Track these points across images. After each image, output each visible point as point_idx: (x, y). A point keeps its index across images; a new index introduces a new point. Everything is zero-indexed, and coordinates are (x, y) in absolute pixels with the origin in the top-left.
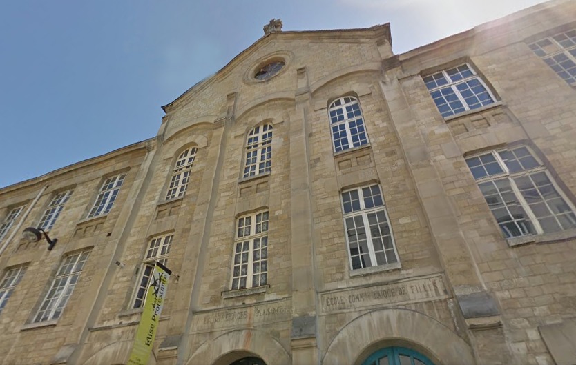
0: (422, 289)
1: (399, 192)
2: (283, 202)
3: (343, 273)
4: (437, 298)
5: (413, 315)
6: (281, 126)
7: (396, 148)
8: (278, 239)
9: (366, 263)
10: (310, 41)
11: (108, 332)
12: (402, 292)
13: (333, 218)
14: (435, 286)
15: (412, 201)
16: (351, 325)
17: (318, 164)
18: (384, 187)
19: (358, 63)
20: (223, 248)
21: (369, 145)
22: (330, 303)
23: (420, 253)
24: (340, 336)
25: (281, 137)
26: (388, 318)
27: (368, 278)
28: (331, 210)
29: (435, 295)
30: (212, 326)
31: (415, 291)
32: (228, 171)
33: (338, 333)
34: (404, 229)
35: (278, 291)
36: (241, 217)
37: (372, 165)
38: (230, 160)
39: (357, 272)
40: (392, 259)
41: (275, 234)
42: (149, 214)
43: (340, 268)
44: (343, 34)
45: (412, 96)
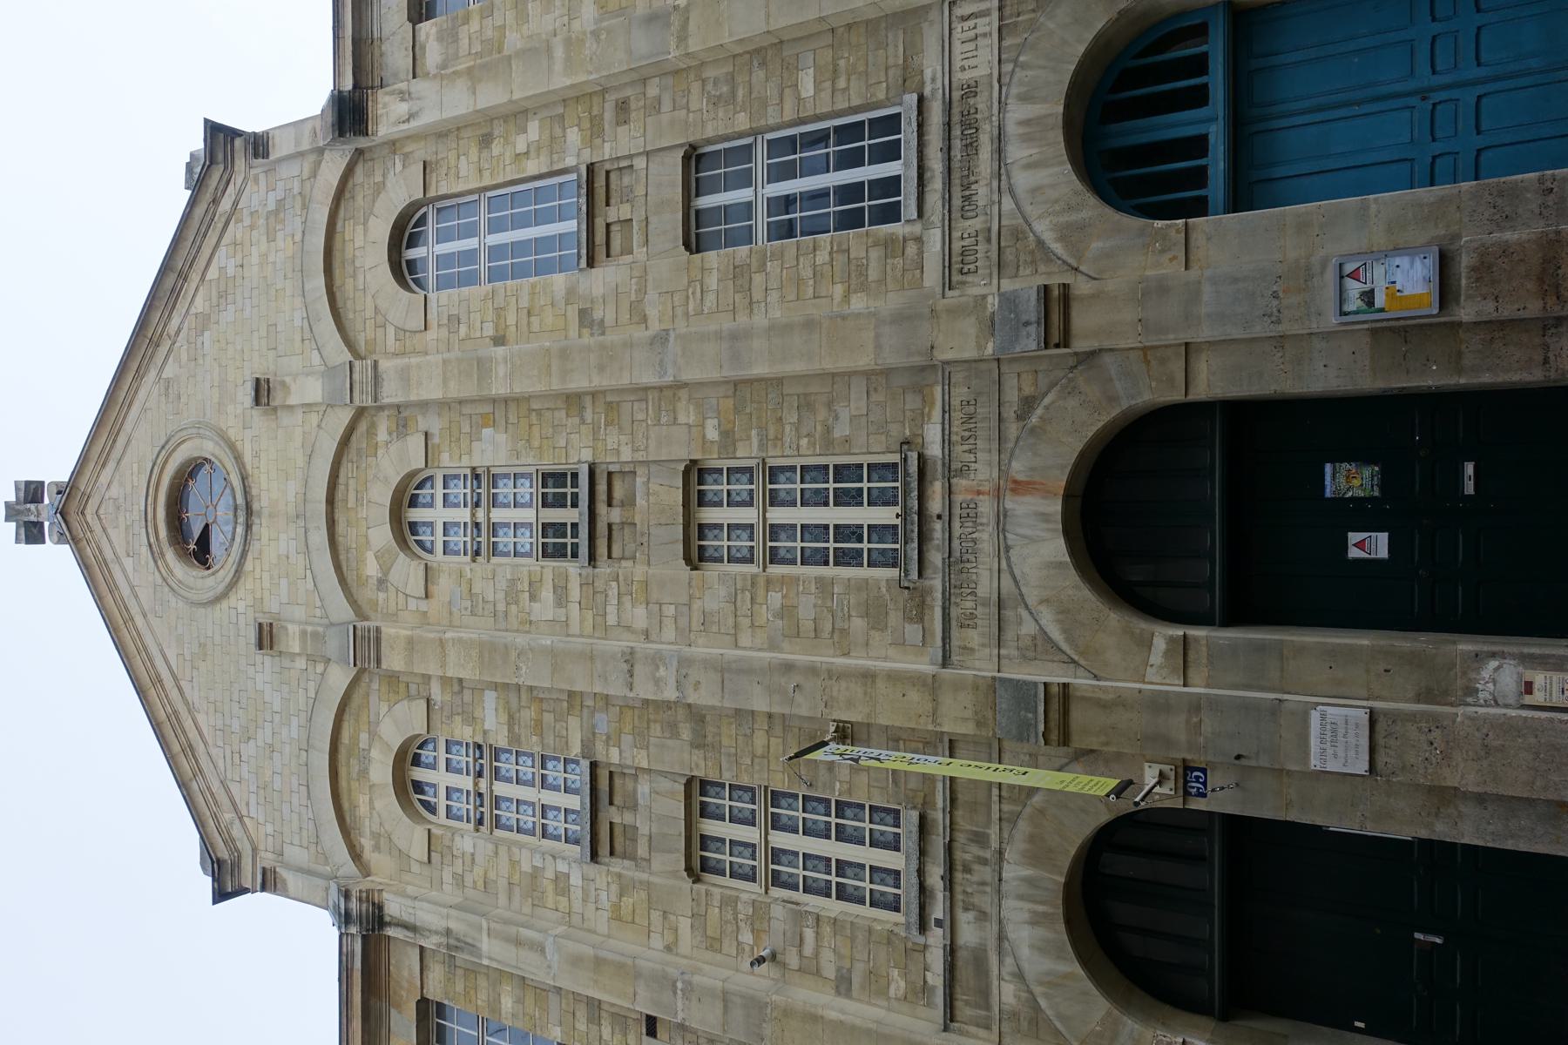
0: (971, 46)
1: (733, 93)
2: (682, 419)
3: (905, 240)
4: (995, 15)
5: (1024, 66)
6: (436, 440)
7: (611, 98)
8: (788, 428)
9: (891, 185)
10: (152, 375)
11: (962, 955)
12: (971, 90)
13: (762, 268)
14: (968, 18)
15: (763, 64)
16: (1028, 209)
17: (597, 314)
18: (710, 132)
19: (298, 220)
20: (775, 598)
21: (586, 467)
22: (972, 267)
23: (891, 49)
24: (1048, 237)
25: (474, 437)
26: (1021, 123)
27: (928, 175)
28: (739, 273)
29: (987, 20)
30: (983, 605)
31: (972, 62)
32: (536, 606)
33: (1040, 243)
34: (828, 84)
35: (922, 417)
36: (697, 864)
37: (640, 163)
38: (501, 607)
39: (909, 209)
40: (893, 123)
41: (771, 435)
42: (614, 888)
43: (891, 247)
44: (162, 715)
45: (477, 48)
